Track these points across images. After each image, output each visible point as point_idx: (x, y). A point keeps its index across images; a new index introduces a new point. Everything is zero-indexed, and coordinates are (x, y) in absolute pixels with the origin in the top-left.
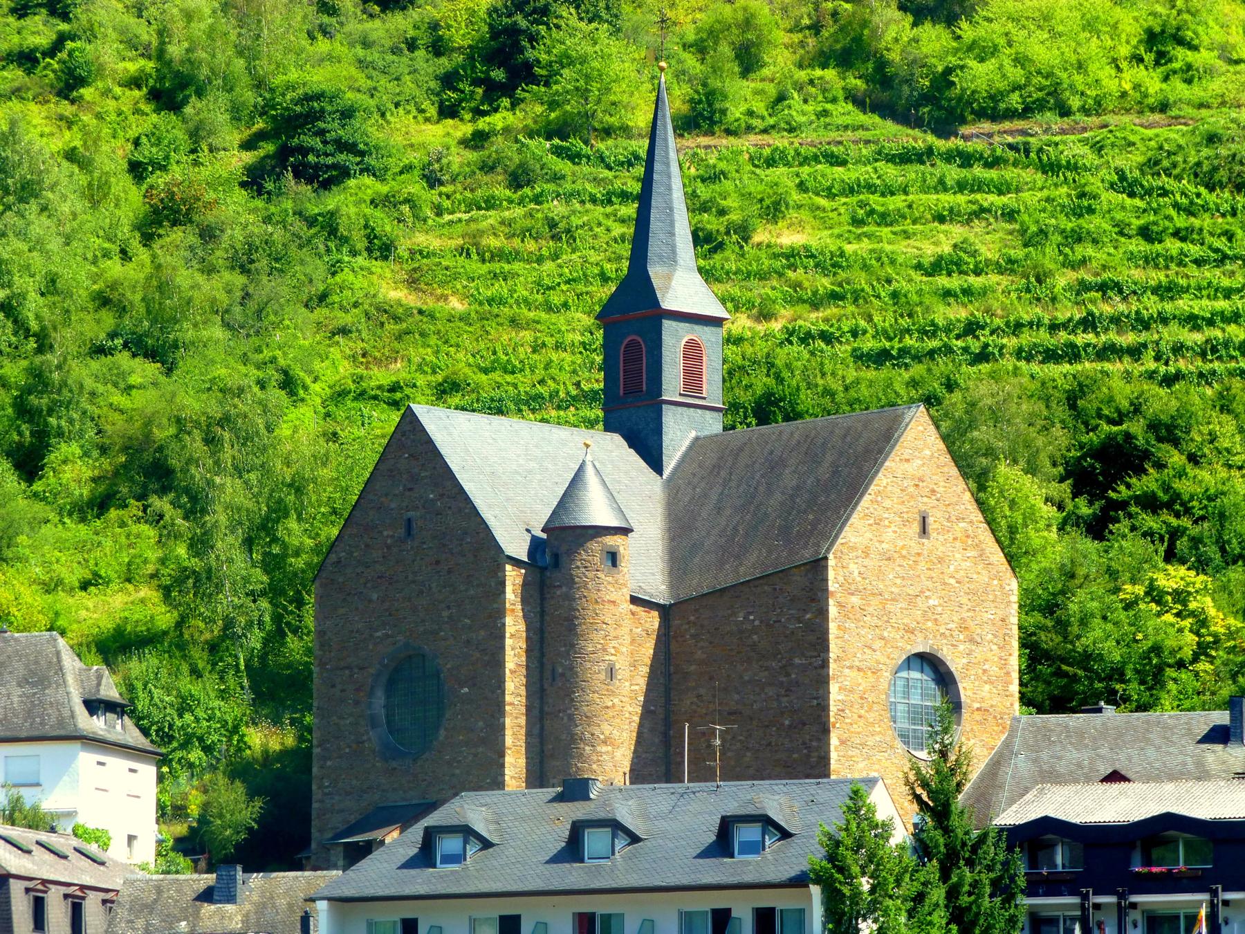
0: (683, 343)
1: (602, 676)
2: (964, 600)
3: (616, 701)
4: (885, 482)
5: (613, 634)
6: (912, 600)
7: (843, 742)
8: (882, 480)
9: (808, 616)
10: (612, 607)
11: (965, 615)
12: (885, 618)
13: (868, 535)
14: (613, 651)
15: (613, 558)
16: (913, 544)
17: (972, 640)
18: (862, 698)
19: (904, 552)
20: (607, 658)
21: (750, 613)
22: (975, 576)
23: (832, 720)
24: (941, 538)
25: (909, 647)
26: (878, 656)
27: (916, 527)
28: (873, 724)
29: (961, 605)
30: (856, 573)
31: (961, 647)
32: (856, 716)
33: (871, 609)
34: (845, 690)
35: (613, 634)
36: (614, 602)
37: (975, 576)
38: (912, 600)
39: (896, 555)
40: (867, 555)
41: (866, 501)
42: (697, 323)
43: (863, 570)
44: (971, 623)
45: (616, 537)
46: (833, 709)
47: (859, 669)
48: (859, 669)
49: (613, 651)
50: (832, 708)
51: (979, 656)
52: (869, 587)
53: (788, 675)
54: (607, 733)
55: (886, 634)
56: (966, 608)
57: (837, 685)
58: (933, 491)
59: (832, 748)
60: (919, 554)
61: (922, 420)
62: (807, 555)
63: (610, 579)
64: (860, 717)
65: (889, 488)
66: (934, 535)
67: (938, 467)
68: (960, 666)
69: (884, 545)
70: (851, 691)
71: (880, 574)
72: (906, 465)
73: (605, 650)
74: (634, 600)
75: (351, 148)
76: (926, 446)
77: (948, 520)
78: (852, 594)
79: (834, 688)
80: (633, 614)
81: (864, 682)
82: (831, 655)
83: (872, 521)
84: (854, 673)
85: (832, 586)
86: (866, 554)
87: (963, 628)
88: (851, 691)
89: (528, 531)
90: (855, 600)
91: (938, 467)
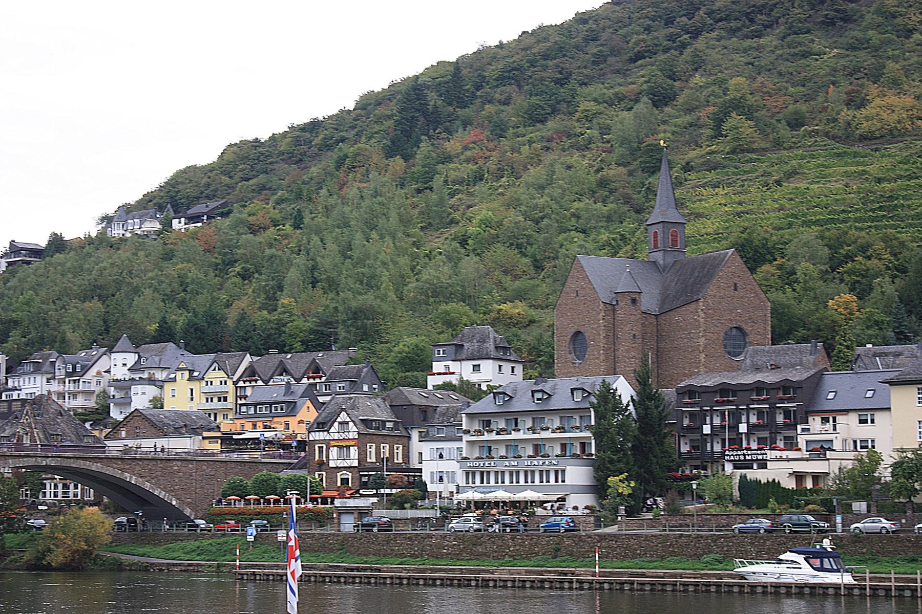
6: (730, 310)
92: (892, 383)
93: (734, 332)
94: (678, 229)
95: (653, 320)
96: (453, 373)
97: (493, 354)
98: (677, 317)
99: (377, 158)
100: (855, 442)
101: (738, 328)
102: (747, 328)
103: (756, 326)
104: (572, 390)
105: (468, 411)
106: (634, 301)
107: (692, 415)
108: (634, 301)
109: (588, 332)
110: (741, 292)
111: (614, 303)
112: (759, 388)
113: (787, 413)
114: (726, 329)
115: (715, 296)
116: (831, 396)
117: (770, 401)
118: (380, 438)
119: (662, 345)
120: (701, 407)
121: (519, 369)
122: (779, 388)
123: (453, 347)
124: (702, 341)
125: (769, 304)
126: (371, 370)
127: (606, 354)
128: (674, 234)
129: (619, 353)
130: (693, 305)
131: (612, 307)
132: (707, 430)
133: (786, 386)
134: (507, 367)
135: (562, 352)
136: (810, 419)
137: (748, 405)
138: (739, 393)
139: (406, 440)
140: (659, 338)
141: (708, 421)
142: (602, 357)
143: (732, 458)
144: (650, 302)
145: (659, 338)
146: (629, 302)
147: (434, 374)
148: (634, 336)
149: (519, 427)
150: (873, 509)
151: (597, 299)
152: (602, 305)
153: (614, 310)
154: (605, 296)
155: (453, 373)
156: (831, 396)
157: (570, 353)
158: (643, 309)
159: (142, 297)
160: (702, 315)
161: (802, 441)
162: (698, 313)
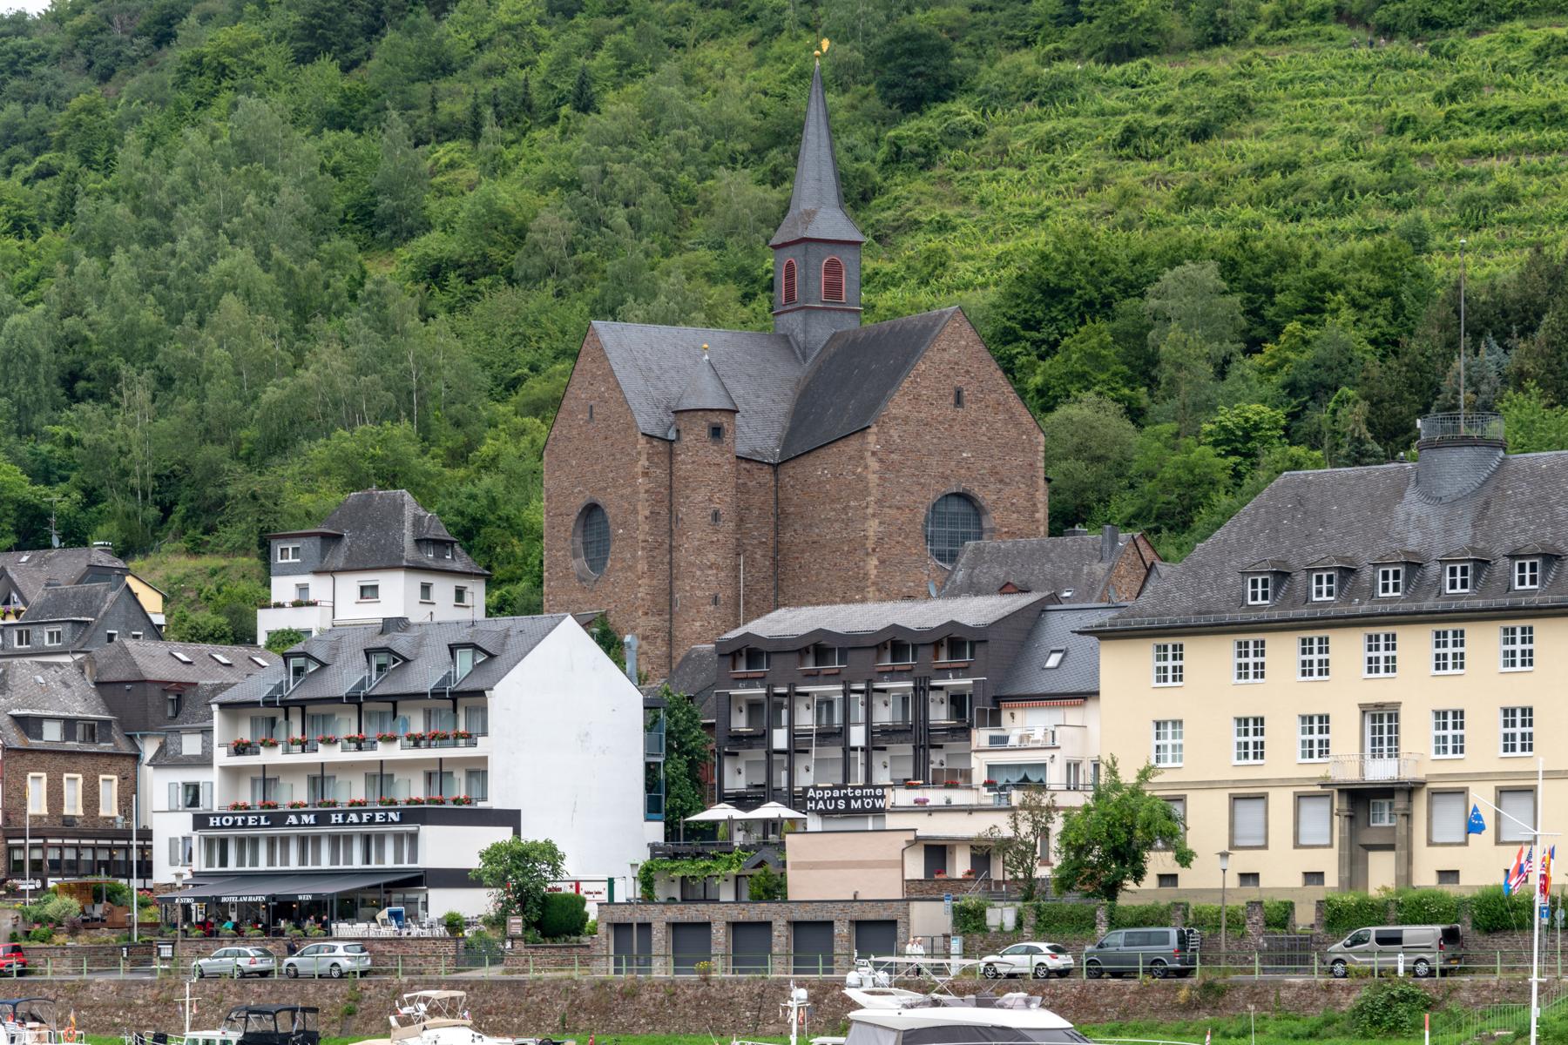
6: (946, 454)
17: (1001, 481)
27: (951, 399)
84: (893, 512)
87: (994, 472)
92: (1105, 634)
93: (955, 507)
94: (844, 256)
95: (766, 476)
96: (314, 604)
97: (409, 552)
98: (819, 469)
99: (275, 59)
100: (1096, 767)
101: (965, 497)
102: (986, 496)
103: (1007, 491)
104: (452, 649)
105: (225, 697)
106: (716, 432)
107: (754, 706)
108: (716, 432)
109: (613, 509)
110: (971, 410)
111: (672, 435)
112: (896, 644)
113: (957, 702)
114: (932, 497)
115: (906, 420)
116: (1053, 661)
117: (917, 672)
118: (60, 760)
119: (787, 536)
120: (770, 687)
121: (477, 593)
122: (807, 650)
123: (318, 541)
124: (873, 527)
125: (1042, 438)
126: (126, 598)
127: (651, 561)
128: (834, 269)
129: (682, 556)
130: (854, 444)
131: (666, 446)
132: (780, 739)
133: (954, 641)
134: (443, 589)
135: (560, 554)
136: (1005, 716)
137: (792, 686)
138: (852, 655)
139: (128, 764)
140: (780, 519)
141: (784, 721)
142: (642, 566)
143: (821, 805)
144: (759, 431)
145: (780, 519)
146: (705, 433)
147: (269, 607)
148: (716, 516)
149: (275, 738)
150: (1030, 920)
151: (631, 425)
152: (642, 441)
153: (671, 455)
154: (647, 418)
155: (314, 604)
156: (1053, 661)
157: (575, 556)
158: (742, 448)
159: (769, 316)
160: (873, 464)
161: (979, 767)
162: (865, 462)
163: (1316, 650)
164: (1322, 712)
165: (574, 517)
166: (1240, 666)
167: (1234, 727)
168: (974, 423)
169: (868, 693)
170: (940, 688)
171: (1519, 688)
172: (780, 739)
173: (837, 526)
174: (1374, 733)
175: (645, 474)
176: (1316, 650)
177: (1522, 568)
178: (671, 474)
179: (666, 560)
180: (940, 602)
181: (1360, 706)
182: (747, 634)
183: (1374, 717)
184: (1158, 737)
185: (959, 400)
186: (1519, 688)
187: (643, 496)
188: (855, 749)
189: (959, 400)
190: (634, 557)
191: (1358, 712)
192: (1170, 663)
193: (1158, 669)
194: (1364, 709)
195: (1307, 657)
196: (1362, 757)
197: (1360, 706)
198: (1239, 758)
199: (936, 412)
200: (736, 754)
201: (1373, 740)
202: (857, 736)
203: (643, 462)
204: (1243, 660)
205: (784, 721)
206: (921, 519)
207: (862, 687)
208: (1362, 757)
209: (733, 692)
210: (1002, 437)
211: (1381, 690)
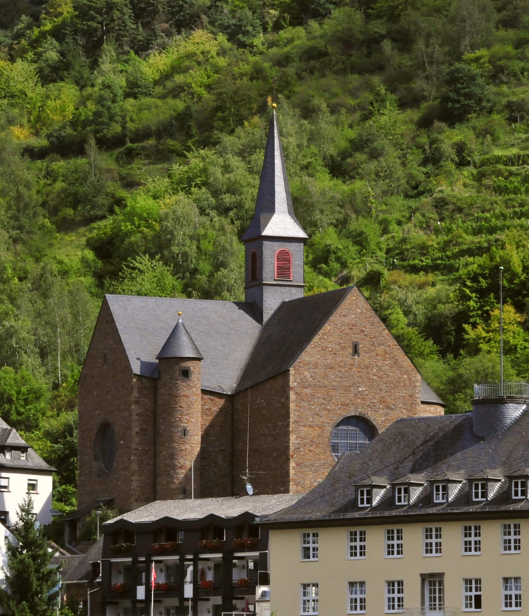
0: (277, 252)
1: (179, 434)
2: (383, 387)
3: (187, 446)
4: (329, 328)
5: (186, 412)
6: (347, 389)
7: (298, 465)
8: (327, 327)
9: (283, 400)
10: (185, 399)
11: (383, 395)
12: (328, 399)
13: (319, 357)
14: (186, 421)
15: (186, 373)
16: (348, 359)
17: (388, 408)
18: (311, 441)
19: (342, 364)
20: (182, 425)
21: (262, 399)
22: (391, 374)
23: (291, 453)
24: (367, 355)
25: (344, 413)
26: (324, 419)
27: (350, 350)
28: (319, 455)
29: (381, 390)
30: (309, 377)
31: (381, 412)
32: (307, 451)
33: (319, 395)
34: (300, 437)
35: (186, 412)
36: (187, 396)
37: (391, 374)
38: (347, 389)
39: (337, 366)
40: (316, 367)
41: (316, 339)
42: (285, 242)
43: (313, 375)
44: (388, 400)
45: (187, 363)
46: (292, 448)
47: (310, 426)
48: (310, 426)
49: (186, 421)
50: (291, 447)
51: (393, 416)
52: (318, 383)
53: (275, 431)
54: (182, 463)
55: (329, 407)
56: (384, 391)
57: (294, 436)
58: (362, 331)
59: (291, 468)
60: (352, 365)
61: (355, 294)
62: (284, 368)
63: (184, 384)
64: (310, 451)
65: (332, 331)
66: (362, 354)
67: (366, 318)
68: (380, 422)
69: (328, 361)
70: (305, 438)
71: (325, 376)
72: (344, 318)
73: (181, 421)
74: (204, 392)
75: (469, 96)
76: (357, 306)
77: (373, 345)
78: (306, 388)
79: (292, 438)
80: (212, 400)
81: (313, 433)
82: (291, 420)
83: (320, 349)
84: (306, 429)
85: (292, 384)
86: (316, 366)
87: (382, 401)
88: (305, 438)
89: (138, 359)
90: (307, 391)
91: (366, 318)
110: (363, 358)
115: (316, 366)
141: (144, 581)
142: (135, 467)
163: (473, 534)
164: (477, 577)
165: (95, 432)
166: (427, 544)
167: (463, 585)
168: (367, 367)
169: (196, 561)
170: (208, 559)
171: (512, 564)
172: (141, 593)
173: (269, 439)
174: (430, 593)
175: (137, 402)
176: (473, 534)
177: (400, 492)
178: (155, 402)
179: (152, 462)
180: (199, 501)
181: (421, 575)
182: (122, 520)
183: (430, 582)
184: (305, 595)
185: (356, 350)
186: (512, 564)
187: (135, 417)
188: (187, 599)
189: (356, 350)
190: (129, 459)
191: (419, 579)
192: (512, 537)
193: (505, 541)
194: (424, 577)
195: (353, 544)
196: (423, 609)
197: (421, 575)
198: (467, 607)
199: (339, 359)
200: (117, 603)
201: (430, 597)
202: (188, 591)
203: (135, 394)
204: (507, 537)
205: (144, 581)
206: (327, 434)
207: (191, 557)
208: (423, 609)
209: (113, 560)
210: (388, 376)
211: (433, 564)
